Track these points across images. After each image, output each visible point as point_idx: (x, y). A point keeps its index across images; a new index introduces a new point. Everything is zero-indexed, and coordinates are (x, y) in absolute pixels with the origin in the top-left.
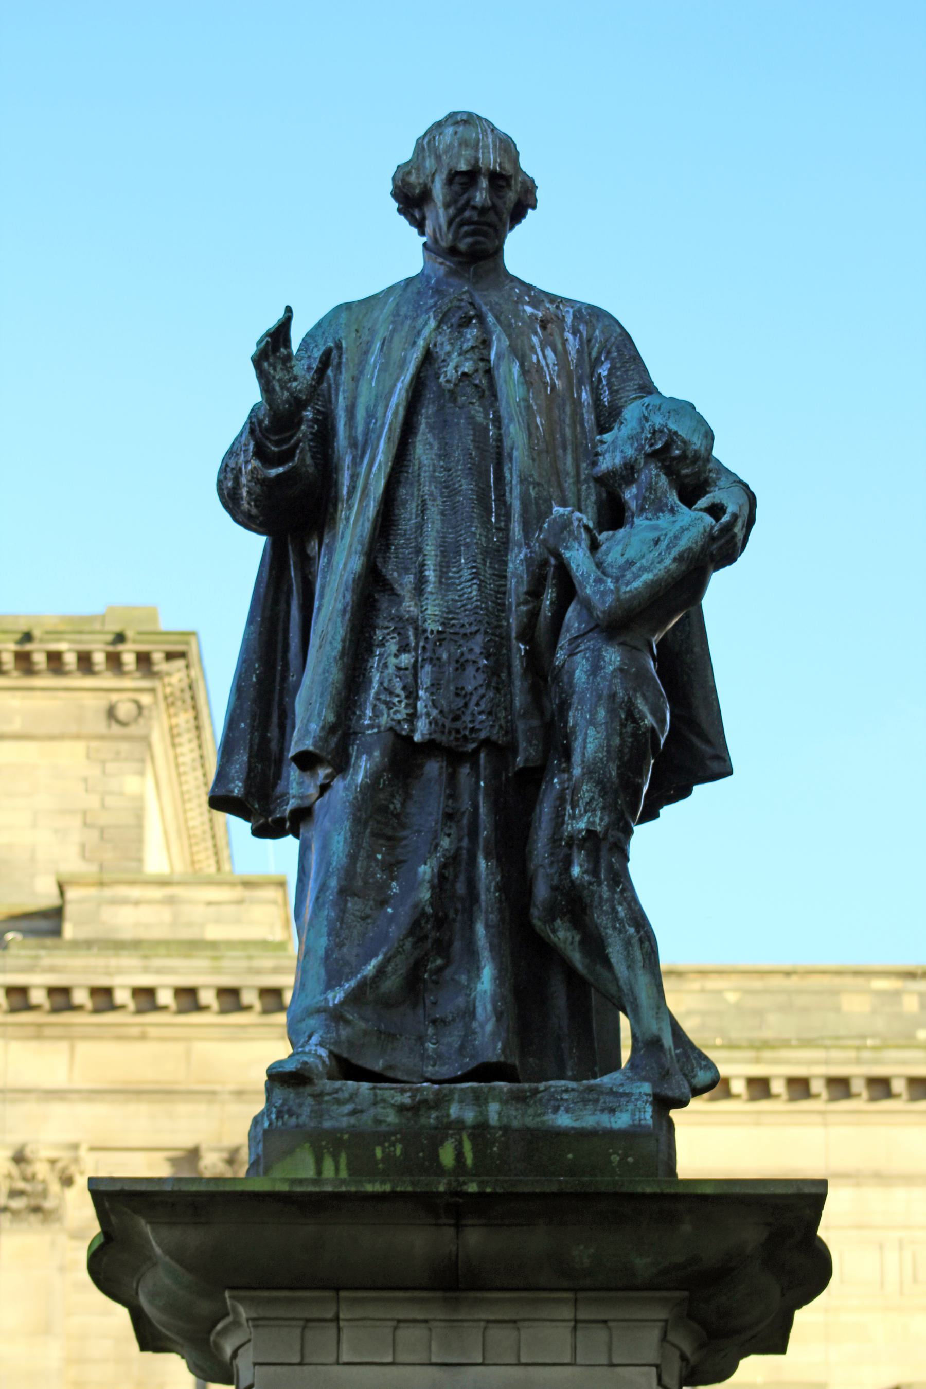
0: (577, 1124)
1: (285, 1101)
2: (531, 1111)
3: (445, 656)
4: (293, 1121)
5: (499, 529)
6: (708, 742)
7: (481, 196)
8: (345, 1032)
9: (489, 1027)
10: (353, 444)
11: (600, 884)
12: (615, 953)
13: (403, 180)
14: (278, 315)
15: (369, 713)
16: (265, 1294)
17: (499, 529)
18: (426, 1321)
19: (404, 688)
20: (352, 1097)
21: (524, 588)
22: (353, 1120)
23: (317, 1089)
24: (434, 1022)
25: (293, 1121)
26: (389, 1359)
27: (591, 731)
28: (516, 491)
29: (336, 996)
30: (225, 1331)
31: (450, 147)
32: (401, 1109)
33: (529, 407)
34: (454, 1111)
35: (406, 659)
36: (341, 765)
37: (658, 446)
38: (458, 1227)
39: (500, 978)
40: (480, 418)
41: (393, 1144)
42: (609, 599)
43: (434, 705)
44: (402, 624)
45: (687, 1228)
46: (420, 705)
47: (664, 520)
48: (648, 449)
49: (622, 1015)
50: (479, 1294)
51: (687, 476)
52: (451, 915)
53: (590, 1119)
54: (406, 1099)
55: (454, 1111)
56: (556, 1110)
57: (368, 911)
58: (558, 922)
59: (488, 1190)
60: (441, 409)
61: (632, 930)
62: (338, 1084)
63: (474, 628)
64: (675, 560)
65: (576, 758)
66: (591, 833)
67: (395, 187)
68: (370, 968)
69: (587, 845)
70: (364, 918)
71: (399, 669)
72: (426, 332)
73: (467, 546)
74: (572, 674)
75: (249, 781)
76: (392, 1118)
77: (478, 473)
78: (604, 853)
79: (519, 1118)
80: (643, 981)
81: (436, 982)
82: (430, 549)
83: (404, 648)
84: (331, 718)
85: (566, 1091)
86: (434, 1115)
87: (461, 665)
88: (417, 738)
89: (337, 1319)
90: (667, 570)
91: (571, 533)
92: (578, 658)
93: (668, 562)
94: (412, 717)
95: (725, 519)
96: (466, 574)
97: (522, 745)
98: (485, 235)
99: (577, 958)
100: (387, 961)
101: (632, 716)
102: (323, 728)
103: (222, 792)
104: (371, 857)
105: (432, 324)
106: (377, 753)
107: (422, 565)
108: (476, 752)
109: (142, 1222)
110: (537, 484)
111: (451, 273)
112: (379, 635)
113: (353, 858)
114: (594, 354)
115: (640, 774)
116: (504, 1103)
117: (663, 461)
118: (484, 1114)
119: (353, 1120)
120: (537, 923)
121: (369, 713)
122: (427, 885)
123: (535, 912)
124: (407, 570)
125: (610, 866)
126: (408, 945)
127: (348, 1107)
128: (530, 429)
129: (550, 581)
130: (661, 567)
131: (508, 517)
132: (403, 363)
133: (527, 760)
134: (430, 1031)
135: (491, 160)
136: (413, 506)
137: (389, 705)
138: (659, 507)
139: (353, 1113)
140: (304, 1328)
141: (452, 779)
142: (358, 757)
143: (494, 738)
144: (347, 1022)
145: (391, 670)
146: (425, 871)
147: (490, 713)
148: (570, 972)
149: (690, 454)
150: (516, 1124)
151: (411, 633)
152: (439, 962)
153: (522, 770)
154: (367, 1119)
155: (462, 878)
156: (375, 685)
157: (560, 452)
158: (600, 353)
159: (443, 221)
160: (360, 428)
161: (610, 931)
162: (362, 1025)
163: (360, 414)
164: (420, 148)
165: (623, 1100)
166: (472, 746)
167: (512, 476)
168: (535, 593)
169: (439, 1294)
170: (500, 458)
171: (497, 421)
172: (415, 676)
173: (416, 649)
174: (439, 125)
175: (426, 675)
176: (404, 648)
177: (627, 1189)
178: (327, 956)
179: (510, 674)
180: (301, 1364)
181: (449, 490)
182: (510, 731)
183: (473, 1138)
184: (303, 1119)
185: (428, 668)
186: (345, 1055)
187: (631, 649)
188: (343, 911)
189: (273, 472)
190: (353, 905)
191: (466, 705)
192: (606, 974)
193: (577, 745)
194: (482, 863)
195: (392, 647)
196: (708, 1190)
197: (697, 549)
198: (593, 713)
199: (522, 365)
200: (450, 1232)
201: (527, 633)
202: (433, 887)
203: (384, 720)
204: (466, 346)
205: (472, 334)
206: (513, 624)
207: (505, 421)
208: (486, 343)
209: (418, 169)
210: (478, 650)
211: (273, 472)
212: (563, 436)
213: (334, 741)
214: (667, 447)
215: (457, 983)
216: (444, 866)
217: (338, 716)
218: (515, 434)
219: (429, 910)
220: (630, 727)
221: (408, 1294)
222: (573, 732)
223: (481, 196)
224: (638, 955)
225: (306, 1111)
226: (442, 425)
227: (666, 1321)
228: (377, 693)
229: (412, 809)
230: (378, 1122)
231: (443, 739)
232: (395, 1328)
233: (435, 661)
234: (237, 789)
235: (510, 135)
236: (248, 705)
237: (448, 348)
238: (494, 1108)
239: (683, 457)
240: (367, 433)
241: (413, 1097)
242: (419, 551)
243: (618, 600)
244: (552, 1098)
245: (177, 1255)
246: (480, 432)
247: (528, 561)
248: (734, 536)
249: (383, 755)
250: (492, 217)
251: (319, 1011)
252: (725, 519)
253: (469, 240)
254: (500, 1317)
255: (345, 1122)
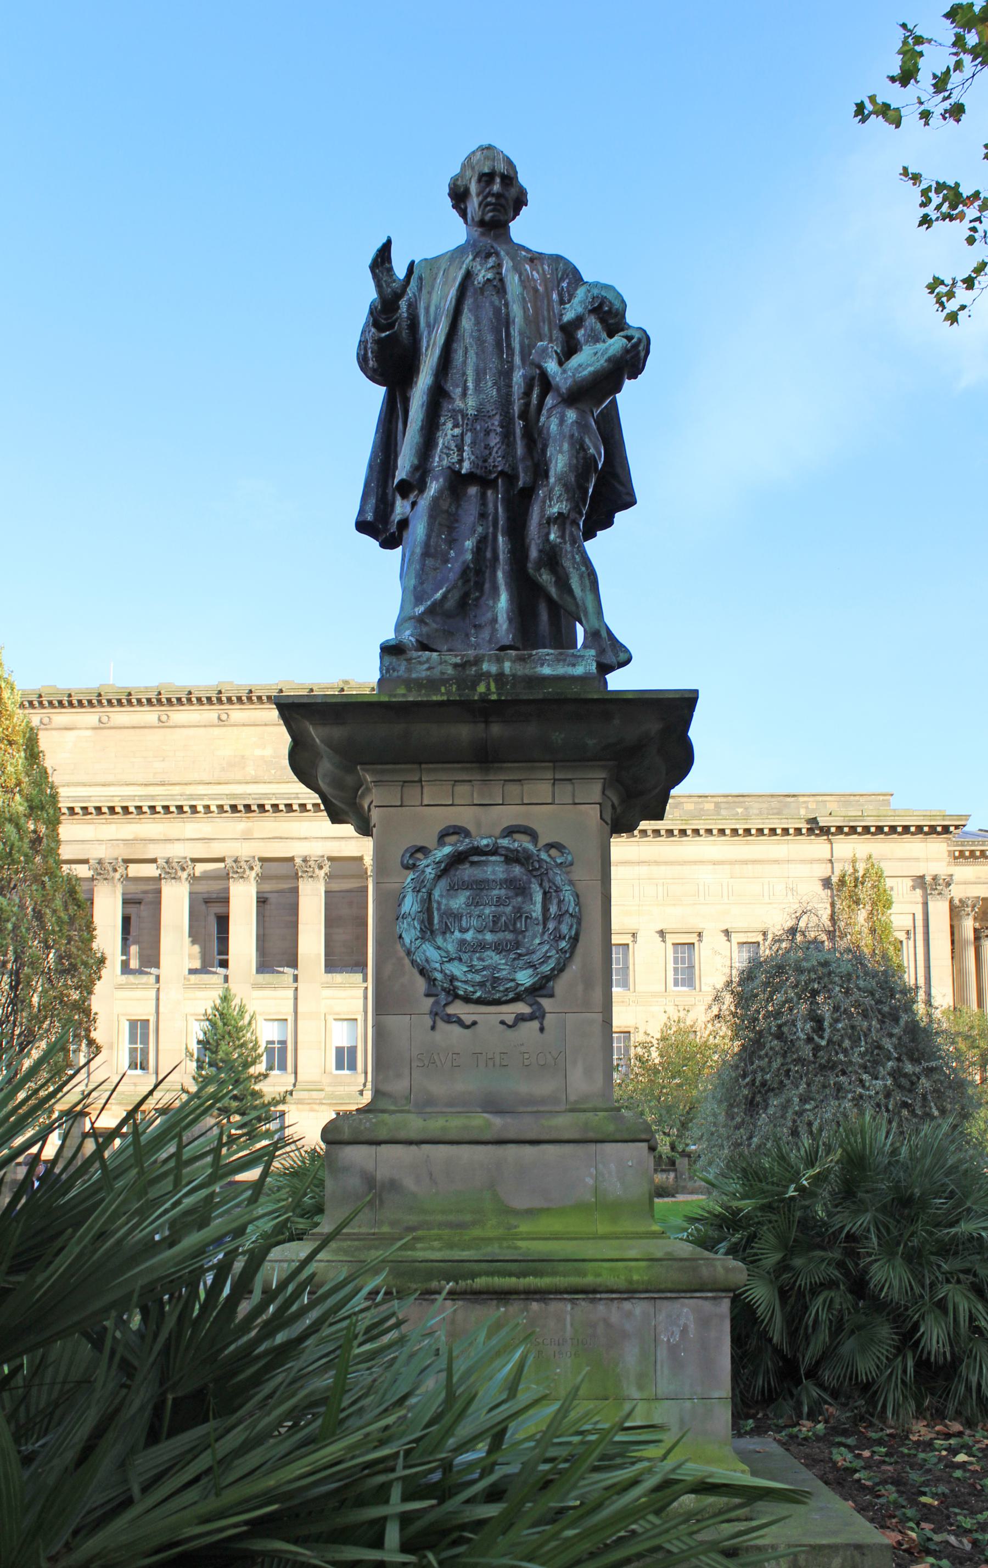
0: (554, 673)
1: (391, 664)
2: (528, 666)
3: (478, 428)
4: (395, 674)
5: (508, 362)
6: (622, 484)
7: (496, 187)
8: (425, 630)
9: (505, 626)
10: (428, 325)
11: (565, 543)
12: (575, 583)
13: (454, 184)
14: (384, 240)
15: (437, 459)
16: (380, 767)
17: (508, 362)
18: (470, 781)
19: (456, 446)
20: (428, 660)
21: (522, 390)
22: (428, 673)
23: (408, 656)
24: (475, 626)
25: (395, 674)
26: (450, 803)
27: (560, 456)
28: (517, 340)
29: (420, 609)
30: (363, 795)
31: (479, 161)
32: (456, 666)
33: (524, 298)
34: (485, 667)
35: (457, 431)
36: (422, 487)
37: (596, 305)
38: (487, 722)
39: (511, 600)
40: (497, 303)
41: (451, 685)
42: (569, 382)
43: (473, 454)
44: (455, 413)
45: (616, 722)
46: (465, 454)
47: (600, 346)
48: (590, 307)
49: (578, 624)
50: (499, 765)
51: (612, 324)
52: (484, 568)
53: (561, 670)
54: (458, 660)
55: (485, 667)
56: (542, 665)
57: (437, 565)
58: (543, 570)
59: (503, 698)
60: (476, 300)
61: (583, 569)
62: (420, 653)
63: (494, 412)
64: (606, 361)
65: (552, 473)
66: (560, 514)
67: (450, 189)
68: (438, 595)
69: (559, 521)
70: (435, 569)
71: (453, 436)
72: (467, 261)
73: (490, 369)
74: (549, 428)
75: (376, 513)
76: (450, 671)
77: (497, 332)
78: (568, 526)
79: (521, 670)
80: (589, 599)
81: (476, 606)
82: (470, 373)
83: (456, 426)
84: (416, 462)
85: (548, 655)
86: (474, 669)
87: (487, 432)
88: (463, 471)
89: (420, 781)
90: (602, 366)
91: (547, 354)
92: (552, 418)
93: (602, 361)
94: (461, 461)
95: (634, 341)
96: (490, 384)
97: (522, 475)
98: (499, 211)
99: (553, 591)
100: (448, 592)
101: (583, 447)
102: (411, 467)
103: (361, 519)
104: (439, 536)
105: (471, 257)
106: (441, 480)
107: (466, 381)
108: (497, 478)
109: (307, 723)
110: (528, 338)
111: (483, 234)
112: (442, 420)
113: (429, 536)
114: (560, 275)
115: (588, 480)
116: (513, 662)
117: (598, 314)
118: (502, 668)
119: (428, 673)
120: (531, 571)
121: (437, 459)
122: (470, 552)
123: (530, 565)
124: (457, 386)
125: (571, 534)
126: (460, 583)
127: (426, 666)
128: (525, 309)
129: (536, 383)
130: (599, 364)
131: (513, 355)
132: (455, 278)
133: (524, 483)
134: (473, 631)
135: (501, 167)
136: (460, 352)
137: (448, 455)
138: (596, 340)
139: (429, 669)
140: (402, 786)
141: (483, 496)
142: (431, 482)
143: (506, 470)
144: (426, 624)
145: (449, 437)
146: (469, 544)
147: (503, 457)
148: (550, 600)
149: (614, 311)
150: (519, 673)
151: (460, 418)
152: (477, 594)
153: (523, 489)
154: (436, 672)
155: (489, 549)
156: (440, 445)
157: (541, 324)
158: (563, 275)
159: (476, 205)
160: (432, 317)
161: (571, 570)
162: (434, 626)
163: (432, 309)
164: (464, 166)
165: (580, 659)
166: (494, 476)
167: (515, 332)
168: (527, 394)
169: (477, 765)
170: (507, 323)
171: (507, 305)
172: (462, 440)
173: (462, 426)
174: (473, 153)
175: (468, 439)
176: (456, 426)
177: (583, 696)
178: (415, 587)
179: (515, 438)
180: (401, 806)
181: (480, 341)
182: (514, 468)
183: (496, 681)
184: (401, 673)
185: (469, 434)
186: (425, 642)
187: (582, 413)
188: (423, 566)
189: (383, 335)
190: (429, 562)
191: (490, 454)
192: (569, 599)
193: (552, 466)
194: (500, 539)
195: (449, 425)
196: (630, 696)
197: (619, 355)
198: (561, 446)
199: (520, 277)
200: (482, 726)
201: (524, 415)
202: (473, 553)
203: (445, 463)
204: (489, 265)
205: (492, 261)
206: (516, 409)
207: (511, 304)
208: (499, 265)
209: (462, 177)
210: (496, 423)
211: (383, 335)
212: (543, 316)
213: (417, 475)
214: (601, 305)
215: (487, 605)
216: (479, 542)
217: (419, 461)
218: (516, 311)
219: (472, 566)
220: (581, 455)
221: (460, 765)
222: (550, 460)
223: (496, 187)
224: (587, 582)
225: (403, 668)
226: (476, 309)
227: (604, 779)
228: (441, 449)
229: (460, 512)
230: (443, 673)
231: (478, 472)
232: (454, 785)
233: (473, 430)
234: (370, 517)
235: (515, 163)
236: (375, 474)
237: (479, 268)
238: (507, 665)
239: (610, 311)
240: (435, 320)
241: (462, 659)
242: (464, 374)
243: (574, 381)
244: (540, 659)
245: (328, 743)
246: (497, 311)
247: (524, 376)
248: (638, 352)
249: (445, 481)
250: (503, 201)
251: (410, 618)
252: (634, 341)
253: (490, 214)
254: (511, 778)
255: (424, 674)
